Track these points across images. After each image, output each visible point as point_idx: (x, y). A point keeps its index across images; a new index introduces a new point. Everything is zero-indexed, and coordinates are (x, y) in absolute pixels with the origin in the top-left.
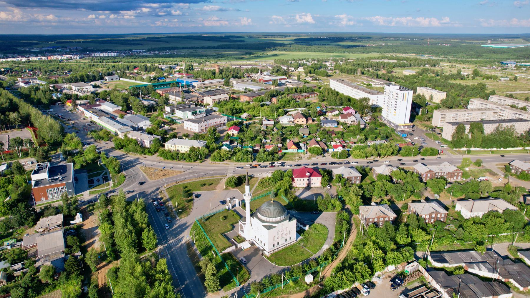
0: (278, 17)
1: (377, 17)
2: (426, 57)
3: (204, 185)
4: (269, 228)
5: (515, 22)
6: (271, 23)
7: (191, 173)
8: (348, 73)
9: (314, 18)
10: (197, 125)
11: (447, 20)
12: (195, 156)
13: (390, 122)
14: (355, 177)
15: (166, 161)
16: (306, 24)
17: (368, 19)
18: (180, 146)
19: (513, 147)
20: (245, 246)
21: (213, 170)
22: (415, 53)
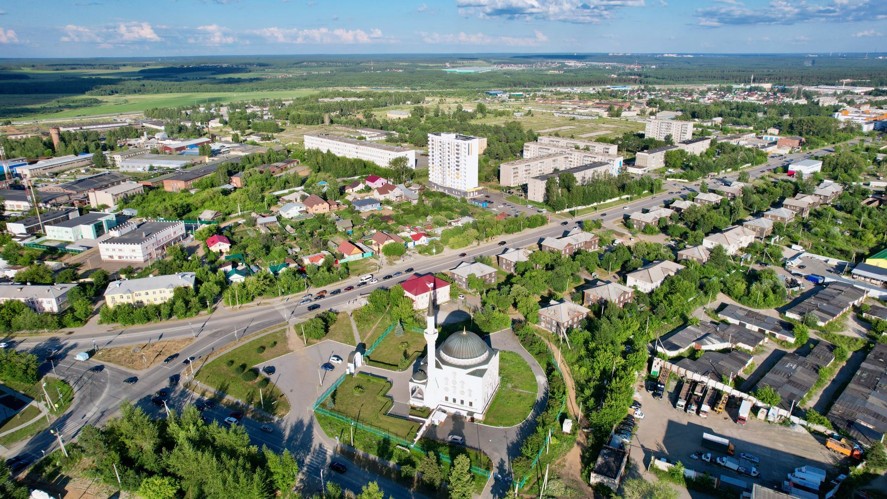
0: (81, 29)
1: (272, 29)
2: (405, 90)
3: (263, 348)
4: (480, 373)
5: (463, 36)
6: (66, 39)
7: (213, 336)
8: (307, 124)
9: (156, 31)
10: (138, 247)
11: (378, 33)
12: (186, 303)
13: (450, 190)
14: (490, 274)
15: (131, 327)
16: (143, 42)
17: (257, 32)
18: (143, 293)
19: (610, 198)
20: (438, 418)
21: (253, 320)
22: (365, 85)
